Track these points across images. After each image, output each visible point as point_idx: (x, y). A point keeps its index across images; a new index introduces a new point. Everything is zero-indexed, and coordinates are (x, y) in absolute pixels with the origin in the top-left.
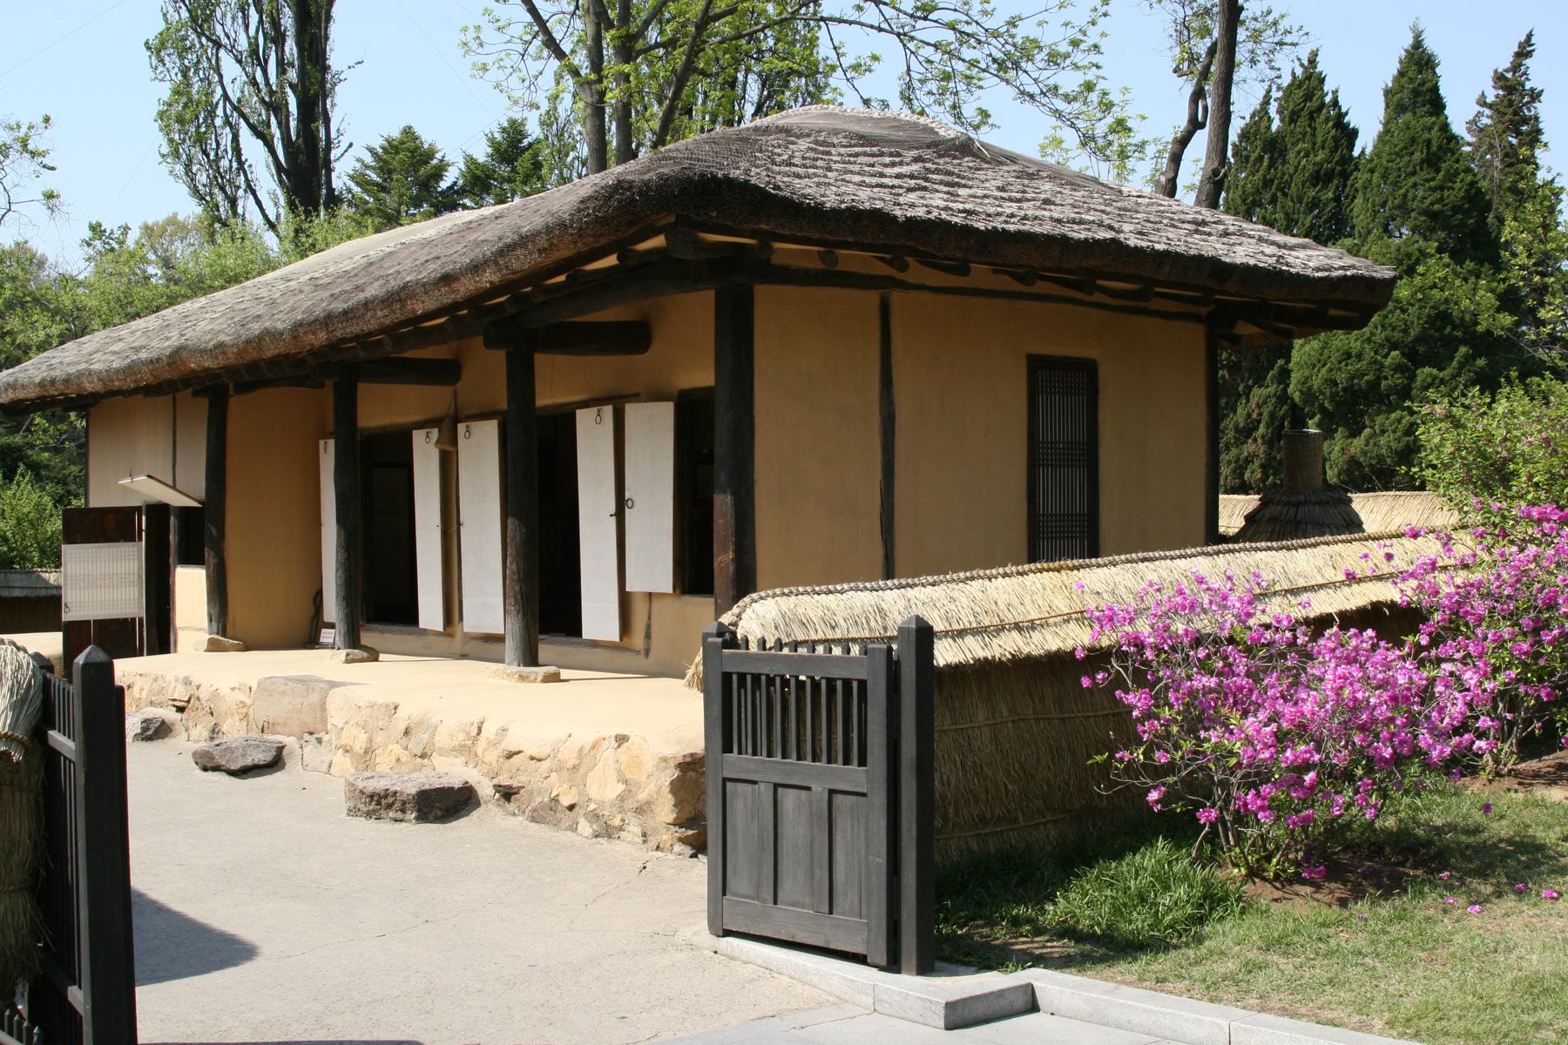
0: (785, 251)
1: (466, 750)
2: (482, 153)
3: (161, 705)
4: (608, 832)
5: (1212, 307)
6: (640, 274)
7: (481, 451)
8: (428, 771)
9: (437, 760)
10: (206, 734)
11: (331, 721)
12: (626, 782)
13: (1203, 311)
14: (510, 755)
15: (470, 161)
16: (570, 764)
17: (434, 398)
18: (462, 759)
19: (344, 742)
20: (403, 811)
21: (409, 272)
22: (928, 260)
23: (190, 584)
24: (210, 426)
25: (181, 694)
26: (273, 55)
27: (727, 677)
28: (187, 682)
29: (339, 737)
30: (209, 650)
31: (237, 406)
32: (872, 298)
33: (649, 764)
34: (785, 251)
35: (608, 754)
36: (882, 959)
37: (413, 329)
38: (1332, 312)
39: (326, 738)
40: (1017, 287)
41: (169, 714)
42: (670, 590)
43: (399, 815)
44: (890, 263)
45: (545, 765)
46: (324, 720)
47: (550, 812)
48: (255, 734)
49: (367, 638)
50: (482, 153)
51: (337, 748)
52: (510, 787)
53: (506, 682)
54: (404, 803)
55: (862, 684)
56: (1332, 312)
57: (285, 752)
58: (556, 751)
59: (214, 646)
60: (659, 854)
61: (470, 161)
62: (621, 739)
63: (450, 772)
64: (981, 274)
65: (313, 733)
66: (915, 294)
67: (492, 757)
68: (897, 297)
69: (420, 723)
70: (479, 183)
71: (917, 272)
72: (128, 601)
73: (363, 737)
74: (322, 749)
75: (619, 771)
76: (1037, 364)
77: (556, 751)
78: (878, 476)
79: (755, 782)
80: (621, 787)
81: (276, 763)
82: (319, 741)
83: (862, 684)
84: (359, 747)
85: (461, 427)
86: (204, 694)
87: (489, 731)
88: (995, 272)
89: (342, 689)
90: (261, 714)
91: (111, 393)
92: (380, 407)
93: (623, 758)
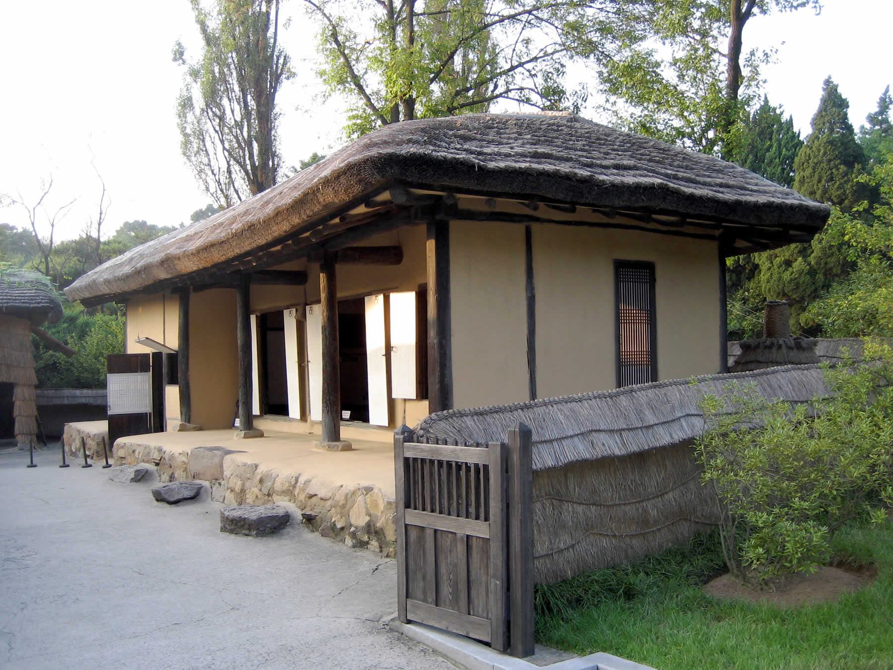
0: (465, 200)
1: (289, 492)
3: (148, 462)
4: (361, 545)
5: (721, 231)
6: (385, 217)
7: (316, 319)
8: (269, 506)
9: (275, 497)
10: (168, 478)
11: (225, 473)
12: (370, 515)
13: (717, 233)
14: (311, 496)
16: (341, 503)
18: (287, 498)
19: (230, 486)
20: (250, 529)
22: (552, 203)
23: (172, 394)
25: (156, 456)
26: (246, 124)
27: (406, 460)
28: (160, 450)
29: (228, 483)
31: (194, 298)
32: (519, 229)
33: (382, 506)
34: (465, 200)
35: (360, 499)
36: (500, 646)
38: (792, 232)
39: (223, 483)
40: (605, 220)
41: (151, 467)
42: (299, 418)
43: (247, 532)
44: (527, 206)
45: (329, 503)
46: (222, 472)
47: (335, 532)
48: (190, 480)
51: (228, 489)
52: (310, 515)
53: (321, 451)
54: (250, 525)
55: (486, 467)
56: (792, 232)
57: (203, 490)
58: (334, 495)
60: (388, 560)
62: (369, 490)
63: (283, 505)
64: (583, 213)
65: (217, 479)
66: (546, 224)
67: (302, 497)
68: (535, 227)
69: (267, 476)
71: (543, 211)
72: (144, 406)
73: (239, 483)
74: (221, 489)
75: (367, 509)
76: (620, 266)
77: (334, 495)
78: (526, 332)
79: (687, 383)
80: (368, 518)
81: (195, 497)
82: (220, 484)
83: (486, 467)
84: (238, 488)
85: (308, 308)
86: (166, 456)
87: (302, 480)
88: (594, 211)
90: (194, 468)
93: (368, 500)
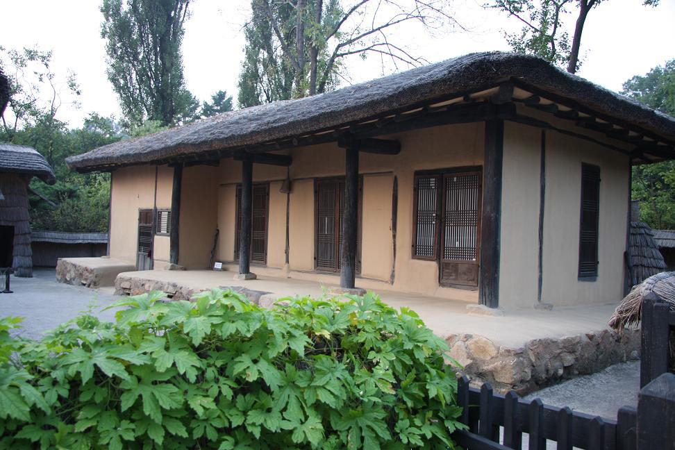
2: (211, 102)
15: (206, 104)
17: (280, 172)
21: (295, 116)
24: (174, 183)
25: (171, 290)
28: (174, 286)
30: (171, 269)
31: (187, 172)
37: (213, 153)
49: (252, 270)
50: (211, 102)
59: (172, 269)
61: (206, 104)
70: (208, 111)
78: (539, 212)
89: (268, 295)
91: (125, 165)
92: (261, 173)
